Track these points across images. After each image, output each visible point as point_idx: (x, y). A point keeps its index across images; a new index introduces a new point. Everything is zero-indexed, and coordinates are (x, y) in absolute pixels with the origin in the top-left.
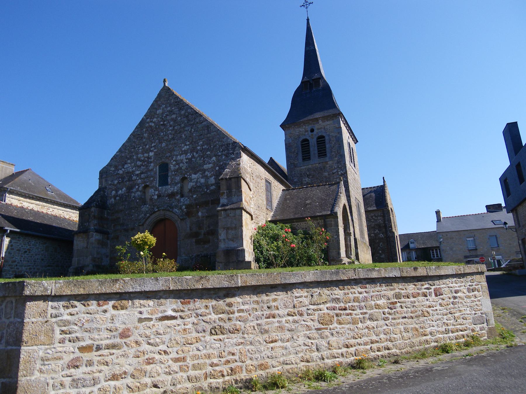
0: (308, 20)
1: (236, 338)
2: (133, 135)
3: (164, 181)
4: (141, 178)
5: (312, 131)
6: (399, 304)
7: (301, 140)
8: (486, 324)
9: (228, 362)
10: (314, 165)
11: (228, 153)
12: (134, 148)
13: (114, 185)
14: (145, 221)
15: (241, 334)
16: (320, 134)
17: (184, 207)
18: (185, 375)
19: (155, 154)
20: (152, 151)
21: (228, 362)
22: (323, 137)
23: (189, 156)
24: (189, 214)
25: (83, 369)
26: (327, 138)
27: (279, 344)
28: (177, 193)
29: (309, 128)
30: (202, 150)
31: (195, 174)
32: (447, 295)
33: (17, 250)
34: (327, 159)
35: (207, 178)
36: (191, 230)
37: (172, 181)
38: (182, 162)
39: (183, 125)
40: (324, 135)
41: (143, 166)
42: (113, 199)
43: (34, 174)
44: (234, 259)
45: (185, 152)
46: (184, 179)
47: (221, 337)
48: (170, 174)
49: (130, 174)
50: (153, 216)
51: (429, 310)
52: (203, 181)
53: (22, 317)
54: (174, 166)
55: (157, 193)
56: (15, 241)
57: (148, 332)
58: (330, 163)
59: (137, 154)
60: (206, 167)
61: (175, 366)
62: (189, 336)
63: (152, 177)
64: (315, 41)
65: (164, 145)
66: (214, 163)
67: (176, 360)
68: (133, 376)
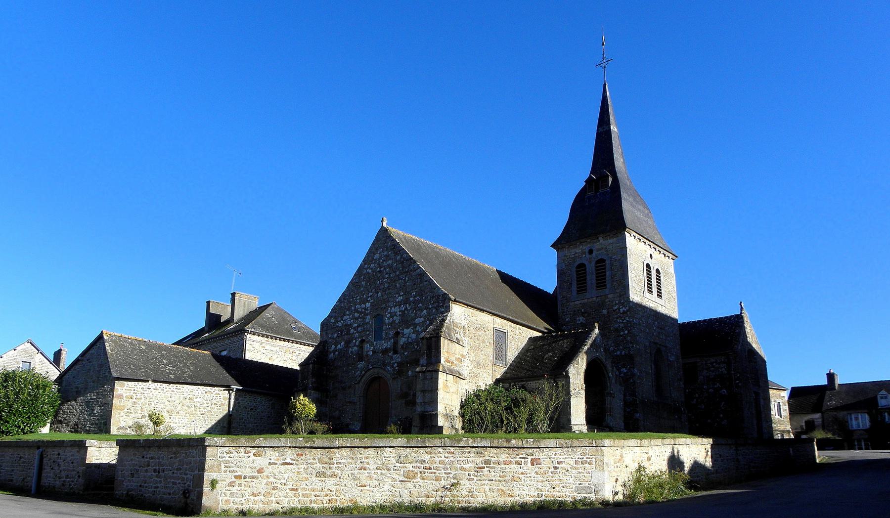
1: (332, 481)
4: (358, 332)
5: (591, 252)
6: (486, 469)
7: (577, 264)
18: (297, 499)
20: (368, 301)
21: (327, 495)
23: (403, 308)
25: (236, 488)
26: (608, 262)
27: (367, 488)
32: (546, 464)
34: (607, 291)
35: (418, 333)
45: (399, 304)
46: (397, 334)
48: (384, 328)
49: (348, 326)
50: (368, 374)
51: (520, 476)
52: (414, 336)
53: (204, 456)
54: (389, 318)
57: (275, 471)
58: (610, 296)
60: (418, 321)
61: (291, 493)
62: (301, 476)
64: (611, 118)
66: (425, 317)
67: (292, 490)
68: (264, 495)
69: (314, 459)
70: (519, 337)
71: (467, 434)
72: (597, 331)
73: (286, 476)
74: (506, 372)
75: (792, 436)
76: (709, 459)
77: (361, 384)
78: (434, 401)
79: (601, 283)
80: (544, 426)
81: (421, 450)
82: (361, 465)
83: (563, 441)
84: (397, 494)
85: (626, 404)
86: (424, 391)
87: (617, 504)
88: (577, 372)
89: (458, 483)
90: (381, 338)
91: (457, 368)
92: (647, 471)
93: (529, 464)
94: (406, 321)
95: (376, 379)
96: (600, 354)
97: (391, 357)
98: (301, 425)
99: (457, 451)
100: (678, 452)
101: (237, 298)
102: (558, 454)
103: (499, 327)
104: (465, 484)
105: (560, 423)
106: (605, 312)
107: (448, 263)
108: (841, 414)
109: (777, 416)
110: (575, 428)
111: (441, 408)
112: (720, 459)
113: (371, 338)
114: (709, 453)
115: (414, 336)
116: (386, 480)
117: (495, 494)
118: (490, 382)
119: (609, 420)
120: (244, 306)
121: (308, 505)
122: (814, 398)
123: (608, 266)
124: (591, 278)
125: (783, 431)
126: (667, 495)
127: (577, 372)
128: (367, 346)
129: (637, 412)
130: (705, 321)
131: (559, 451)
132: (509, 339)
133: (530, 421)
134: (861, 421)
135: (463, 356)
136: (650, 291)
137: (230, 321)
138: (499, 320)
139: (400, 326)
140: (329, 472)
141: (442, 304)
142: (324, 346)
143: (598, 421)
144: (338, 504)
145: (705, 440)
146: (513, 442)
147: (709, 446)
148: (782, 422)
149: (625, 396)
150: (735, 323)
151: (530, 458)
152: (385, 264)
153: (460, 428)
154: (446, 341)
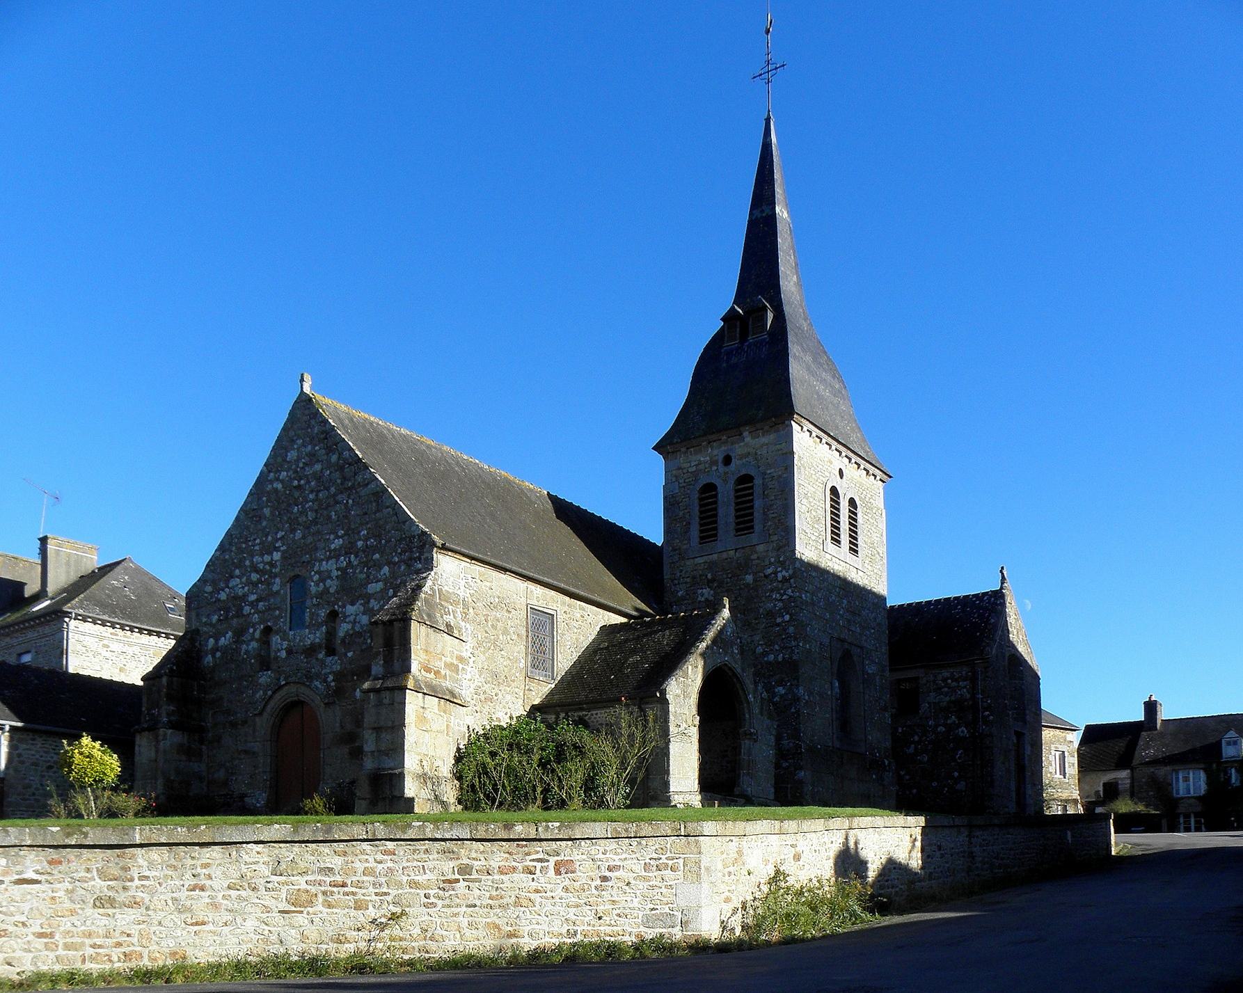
2: (244, 510)
4: (258, 612)
5: (727, 460)
8: (679, 927)
9: (119, 945)
10: (725, 555)
11: (411, 559)
12: (246, 542)
13: (211, 625)
14: (265, 706)
15: (143, 910)
16: (743, 472)
17: (331, 678)
19: (284, 558)
20: (277, 549)
21: (119, 945)
23: (343, 562)
26: (758, 482)
27: (210, 927)
28: (320, 646)
29: (718, 452)
30: (368, 550)
31: (353, 604)
32: (585, 872)
33: (33, 764)
34: (754, 538)
35: (371, 612)
36: (342, 727)
37: (312, 619)
38: (330, 577)
39: (333, 490)
41: (261, 582)
42: (210, 658)
43: (139, 571)
44: (375, 790)
45: (336, 555)
46: (333, 615)
47: (110, 911)
48: (308, 603)
49: (239, 600)
50: (278, 696)
51: (533, 896)
52: (365, 619)
54: (317, 585)
55: (285, 644)
56: (24, 746)
58: (761, 548)
59: (253, 556)
63: (278, 608)
64: (779, 190)
65: (299, 534)
67: (41, 935)
69: (88, 870)
70: (580, 626)
71: (468, 814)
72: (726, 613)
73: (26, 907)
74: (552, 693)
75: (1081, 811)
76: (917, 855)
77: (265, 715)
78: (397, 749)
79: (744, 523)
80: (616, 796)
81: (325, 848)
82: (194, 882)
83: (619, 826)
84: (274, 938)
85: (782, 754)
86: (377, 730)
87: (723, 948)
88: (684, 691)
89: (403, 913)
90: (302, 625)
91: (447, 684)
92: (791, 881)
93: (552, 872)
94: (351, 590)
95: (296, 705)
96: (732, 659)
97: (322, 662)
98: (87, 802)
99: (402, 849)
100: (856, 843)
101: (51, 547)
102: (610, 852)
103: (539, 604)
104: (418, 916)
105: (648, 789)
106: (749, 578)
107: (442, 474)
108: (1162, 771)
109: (1058, 775)
110: (676, 799)
111: (411, 762)
112: (938, 854)
113: (284, 623)
114: (918, 844)
115: (365, 619)
116: (249, 909)
117: (481, 933)
118: (520, 710)
119: (747, 785)
120: (68, 564)
121: (78, 965)
122: (1121, 745)
123: (758, 490)
124: (726, 512)
125: (1067, 801)
126: (825, 924)
127: (684, 691)
128: (276, 639)
129: (801, 768)
130: (938, 601)
131: (612, 845)
132: (561, 626)
133: (590, 785)
134: (1191, 783)
135: (461, 659)
136: (836, 540)
137: (37, 597)
138: (538, 590)
139: (338, 599)
140: (122, 897)
141: (416, 554)
142: (193, 640)
143: (724, 785)
144: (146, 963)
145: (911, 820)
146: (519, 828)
147: (919, 830)
148: (1062, 780)
149: (779, 738)
150: (989, 608)
151: (553, 860)
152: (309, 471)
153: (452, 800)
154: (423, 628)
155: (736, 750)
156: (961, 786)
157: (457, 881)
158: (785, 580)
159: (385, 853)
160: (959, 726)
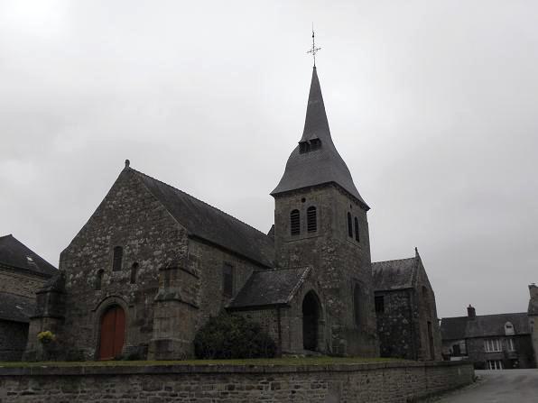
0: (315, 68)
2: (94, 217)
3: (117, 267)
4: (97, 262)
5: (304, 200)
7: (291, 210)
16: (311, 205)
20: (109, 235)
22: (313, 208)
24: (137, 301)
30: (154, 236)
35: (155, 264)
40: (315, 205)
42: (70, 283)
45: (139, 238)
46: (135, 266)
52: (152, 267)
59: (96, 237)
60: (156, 253)
77: (97, 311)
90: (119, 269)
113: (110, 268)
115: (152, 267)
123: (318, 213)
124: (303, 221)
128: (105, 275)
135: (197, 286)
142: (62, 275)
155: (315, 329)
156: (406, 347)
157: (227, 393)
158: (331, 252)
159: (195, 379)
160: (402, 319)
